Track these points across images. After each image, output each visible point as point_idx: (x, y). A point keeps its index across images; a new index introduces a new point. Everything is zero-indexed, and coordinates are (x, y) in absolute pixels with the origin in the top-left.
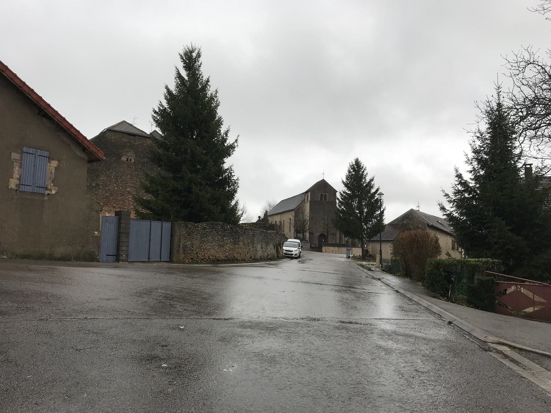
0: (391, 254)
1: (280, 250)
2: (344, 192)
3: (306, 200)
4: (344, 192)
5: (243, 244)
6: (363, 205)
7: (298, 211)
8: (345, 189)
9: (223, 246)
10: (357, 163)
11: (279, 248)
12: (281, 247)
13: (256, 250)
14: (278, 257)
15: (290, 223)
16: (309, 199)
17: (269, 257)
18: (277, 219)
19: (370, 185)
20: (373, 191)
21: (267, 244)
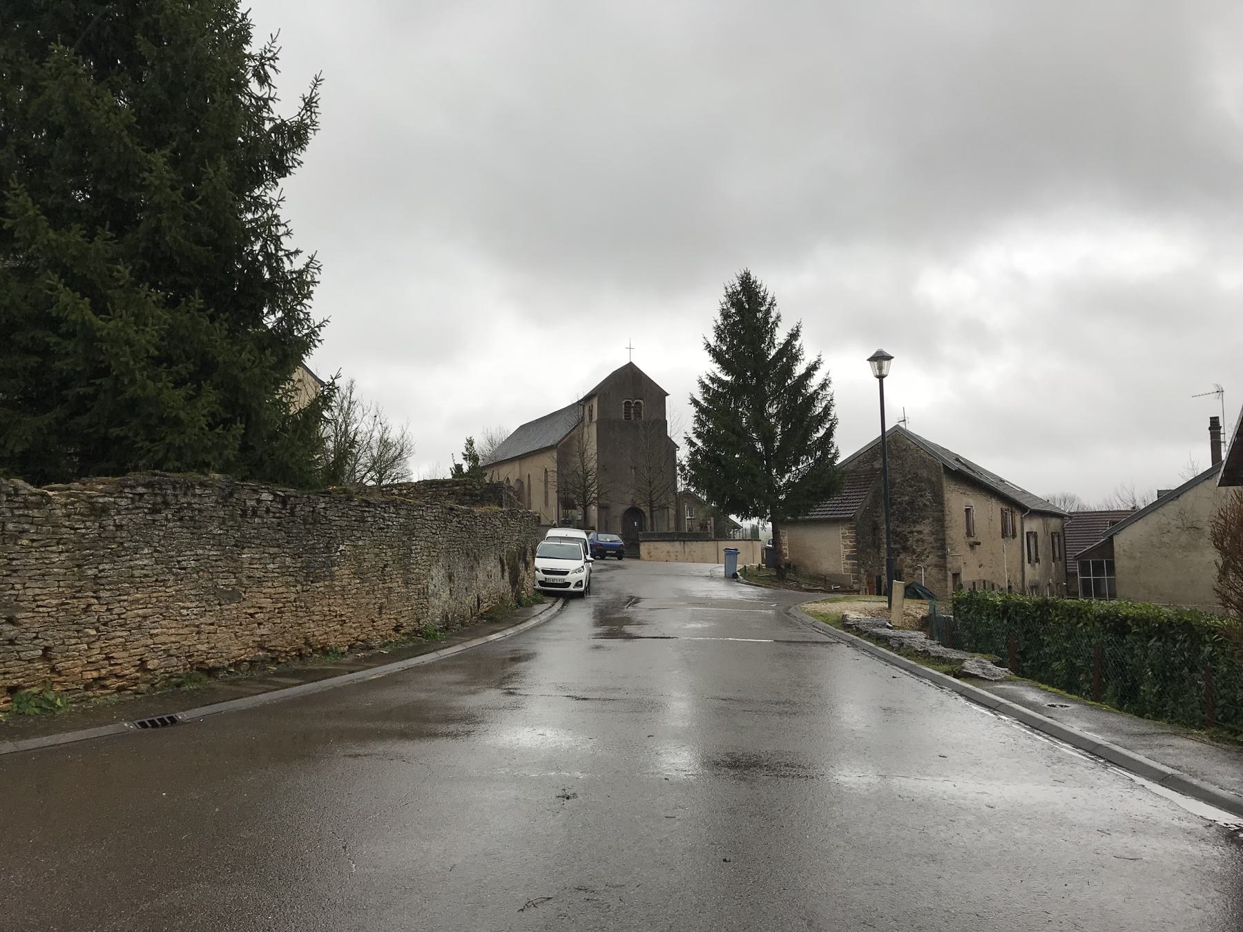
0: (848, 557)
1: (523, 573)
2: (713, 380)
3: (587, 418)
4: (713, 380)
5: (359, 574)
6: (745, 430)
7: (565, 450)
8: (715, 368)
9: (234, 596)
10: (747, 284)
11: (522, 566)
12: (527, 565)
13: (424, 593)
14: (519, 602)
15: (546, 482)
16: (595, 418)
17: (485, 607)
18: (509, 474)
19: (789, 353)
20: (799, 369)
21: (473, 558)
